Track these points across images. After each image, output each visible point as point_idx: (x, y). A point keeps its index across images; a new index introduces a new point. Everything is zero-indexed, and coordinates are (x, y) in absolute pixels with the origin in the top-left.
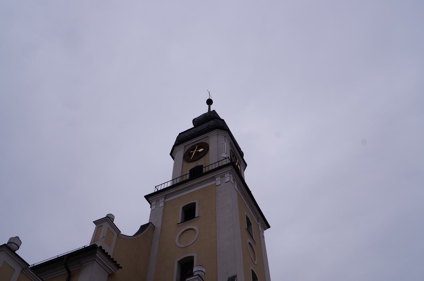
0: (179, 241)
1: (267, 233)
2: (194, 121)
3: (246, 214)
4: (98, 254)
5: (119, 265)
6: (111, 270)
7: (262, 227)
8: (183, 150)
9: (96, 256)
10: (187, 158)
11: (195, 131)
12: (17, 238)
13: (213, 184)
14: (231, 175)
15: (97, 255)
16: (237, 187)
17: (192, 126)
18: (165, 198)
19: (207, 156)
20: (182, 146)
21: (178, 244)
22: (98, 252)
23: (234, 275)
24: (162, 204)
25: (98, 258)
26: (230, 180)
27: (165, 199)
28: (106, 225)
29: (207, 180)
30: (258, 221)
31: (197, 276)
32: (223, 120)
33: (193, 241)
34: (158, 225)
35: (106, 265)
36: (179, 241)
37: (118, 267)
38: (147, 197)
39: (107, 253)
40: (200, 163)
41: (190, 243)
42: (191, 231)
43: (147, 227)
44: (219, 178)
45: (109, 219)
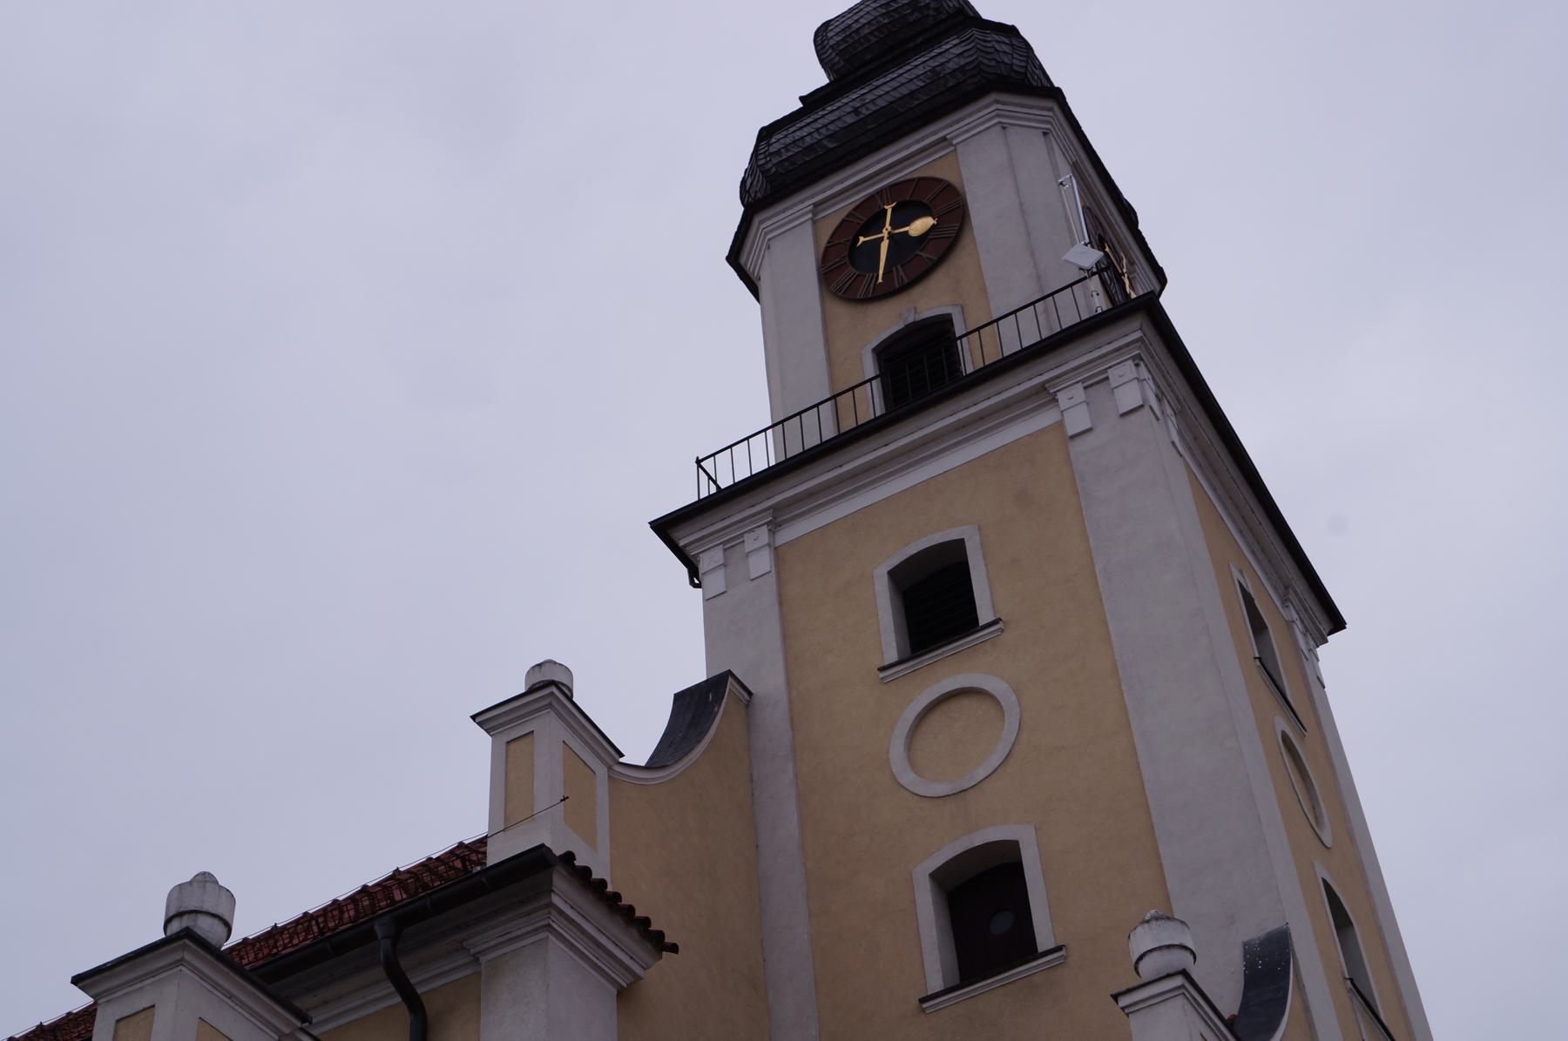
0: (913, 765)
1: (1332, 656)
2: (828, 41)
3: (1236, 575)
4: (563, 895)
5: (661, 934)
6: (628, 969)
7: (1306, 631)
8: (807, 232)
9: (551, 905)
10: (846, 272)
11: (856, 111)
12: (205, 879)
13: (1043, 431)
14: (1144, 374)
15: (556, 900)
16: (1179, 432)
17: (818, 78)
18: (775, 526)
19: (961, 258)
20: (799, 206)
21: (908, 778)
22: (560, 881)
23: (1272, 926)
24: (762, 563)
25: (561, 913)
26: (1145, 399)
27: (772, 532)
28: (548, 730)
29: (1006, 406)
31: (1179, 981)
33: (995, 760)
34: (766, 678)
35: (599, 945)
37: (659, 943)
38: (665, 527)
39: (603, 883)
40: (926, 302)
41: (981, 773)
42: (966, 703)
43: (718, 699)
44: (1078, 392)
45: (549, 690)
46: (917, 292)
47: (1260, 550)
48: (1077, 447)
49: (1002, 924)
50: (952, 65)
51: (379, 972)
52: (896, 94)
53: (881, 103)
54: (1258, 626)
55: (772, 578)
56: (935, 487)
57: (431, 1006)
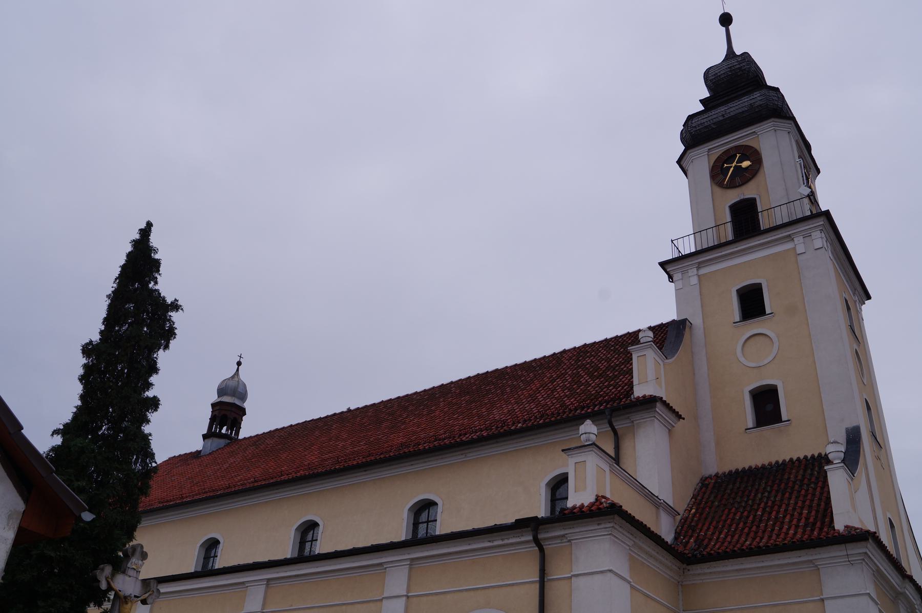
10: (718, 174)
11: (723, 116)
14: (823, 235)
18: (698, 268)
19: (759, 178)
21: (742, 359)
24: (694, 280)
30: (854, 294)
32: (777, 90)
33: (770, 358)
34: (696, 320)
36: (742, 349)
37: (679, 417)
38: (663, 265)
40: (747, 192)
41: (766, 362)
42: (761, 338)
44: (801, 239)
46: (744, 187)
47: (854, 290)
48: (800, 258)
49: (769, 407)
50: (757, 104)
51: (606, 421)
52: (737, 112)
53: (732, 114)
54: (848, 308)
55: (698, 286)
56: (752, 263)
57: (620, 432)
